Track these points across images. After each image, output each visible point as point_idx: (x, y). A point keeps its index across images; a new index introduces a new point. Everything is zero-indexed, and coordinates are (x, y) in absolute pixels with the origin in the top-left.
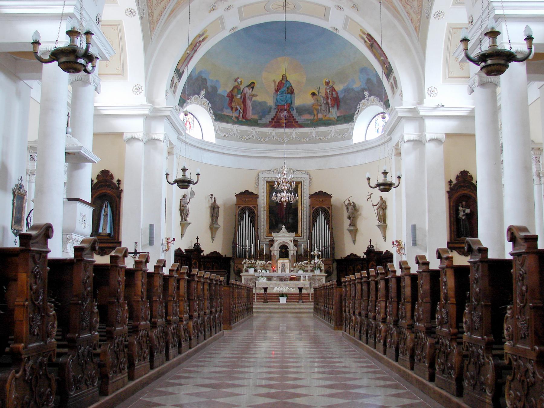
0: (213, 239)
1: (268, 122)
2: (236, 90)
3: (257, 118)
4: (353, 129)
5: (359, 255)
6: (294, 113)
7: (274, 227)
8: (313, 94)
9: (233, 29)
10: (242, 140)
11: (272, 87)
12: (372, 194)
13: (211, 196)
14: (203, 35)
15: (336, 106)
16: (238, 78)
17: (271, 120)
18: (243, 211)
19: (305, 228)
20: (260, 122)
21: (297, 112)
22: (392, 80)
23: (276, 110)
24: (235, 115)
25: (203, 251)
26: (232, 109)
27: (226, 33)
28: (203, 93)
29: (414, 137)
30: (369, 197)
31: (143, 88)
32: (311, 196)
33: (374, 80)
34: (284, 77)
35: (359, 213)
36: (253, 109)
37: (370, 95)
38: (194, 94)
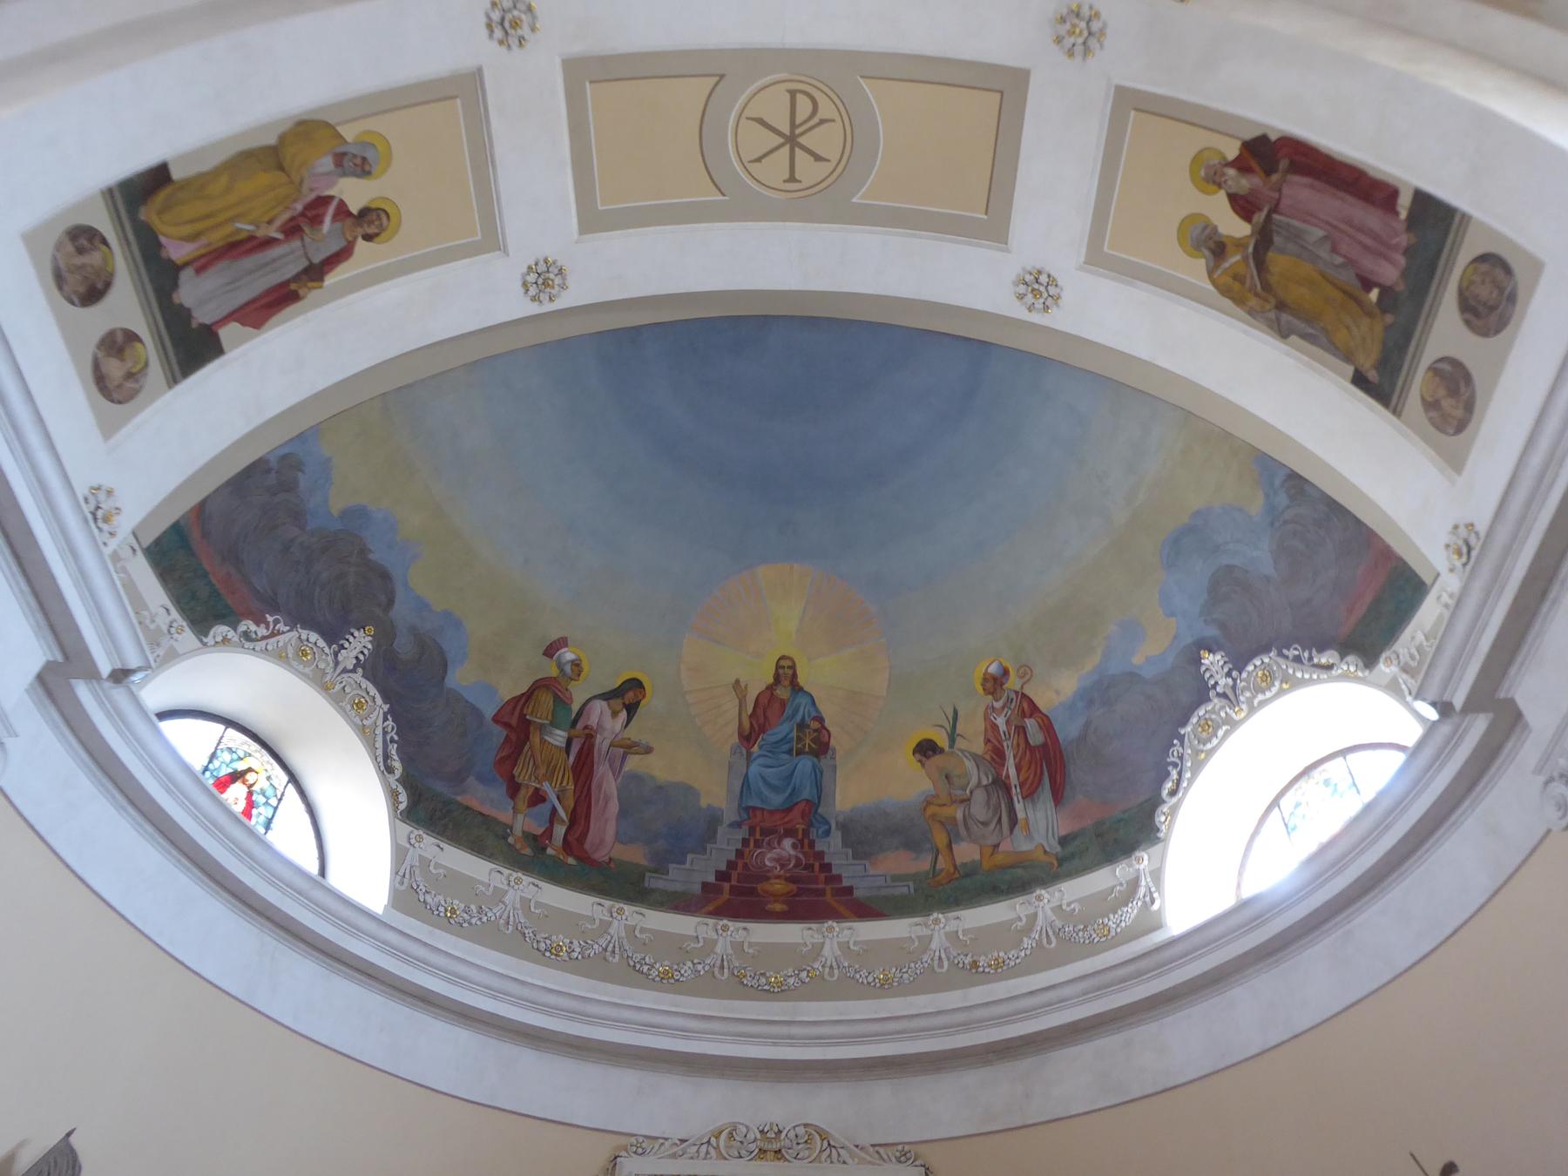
1: (697, 888)
2: (546, 700)
3: (644, 862)
4: (1157, 875)
6: (833, 847)
8: (926, 749)
11: (727, 722)
16: (562, 643)
17: (711, 879)
20: (653, 882)
21: (845, 844)
23: (742, 833)
24: (524, 822)
26: (514, 789)
28: (360, 643)
34: (786, 673)
36: (623, 813)
37: (1238, 662)
38: (301, 618)
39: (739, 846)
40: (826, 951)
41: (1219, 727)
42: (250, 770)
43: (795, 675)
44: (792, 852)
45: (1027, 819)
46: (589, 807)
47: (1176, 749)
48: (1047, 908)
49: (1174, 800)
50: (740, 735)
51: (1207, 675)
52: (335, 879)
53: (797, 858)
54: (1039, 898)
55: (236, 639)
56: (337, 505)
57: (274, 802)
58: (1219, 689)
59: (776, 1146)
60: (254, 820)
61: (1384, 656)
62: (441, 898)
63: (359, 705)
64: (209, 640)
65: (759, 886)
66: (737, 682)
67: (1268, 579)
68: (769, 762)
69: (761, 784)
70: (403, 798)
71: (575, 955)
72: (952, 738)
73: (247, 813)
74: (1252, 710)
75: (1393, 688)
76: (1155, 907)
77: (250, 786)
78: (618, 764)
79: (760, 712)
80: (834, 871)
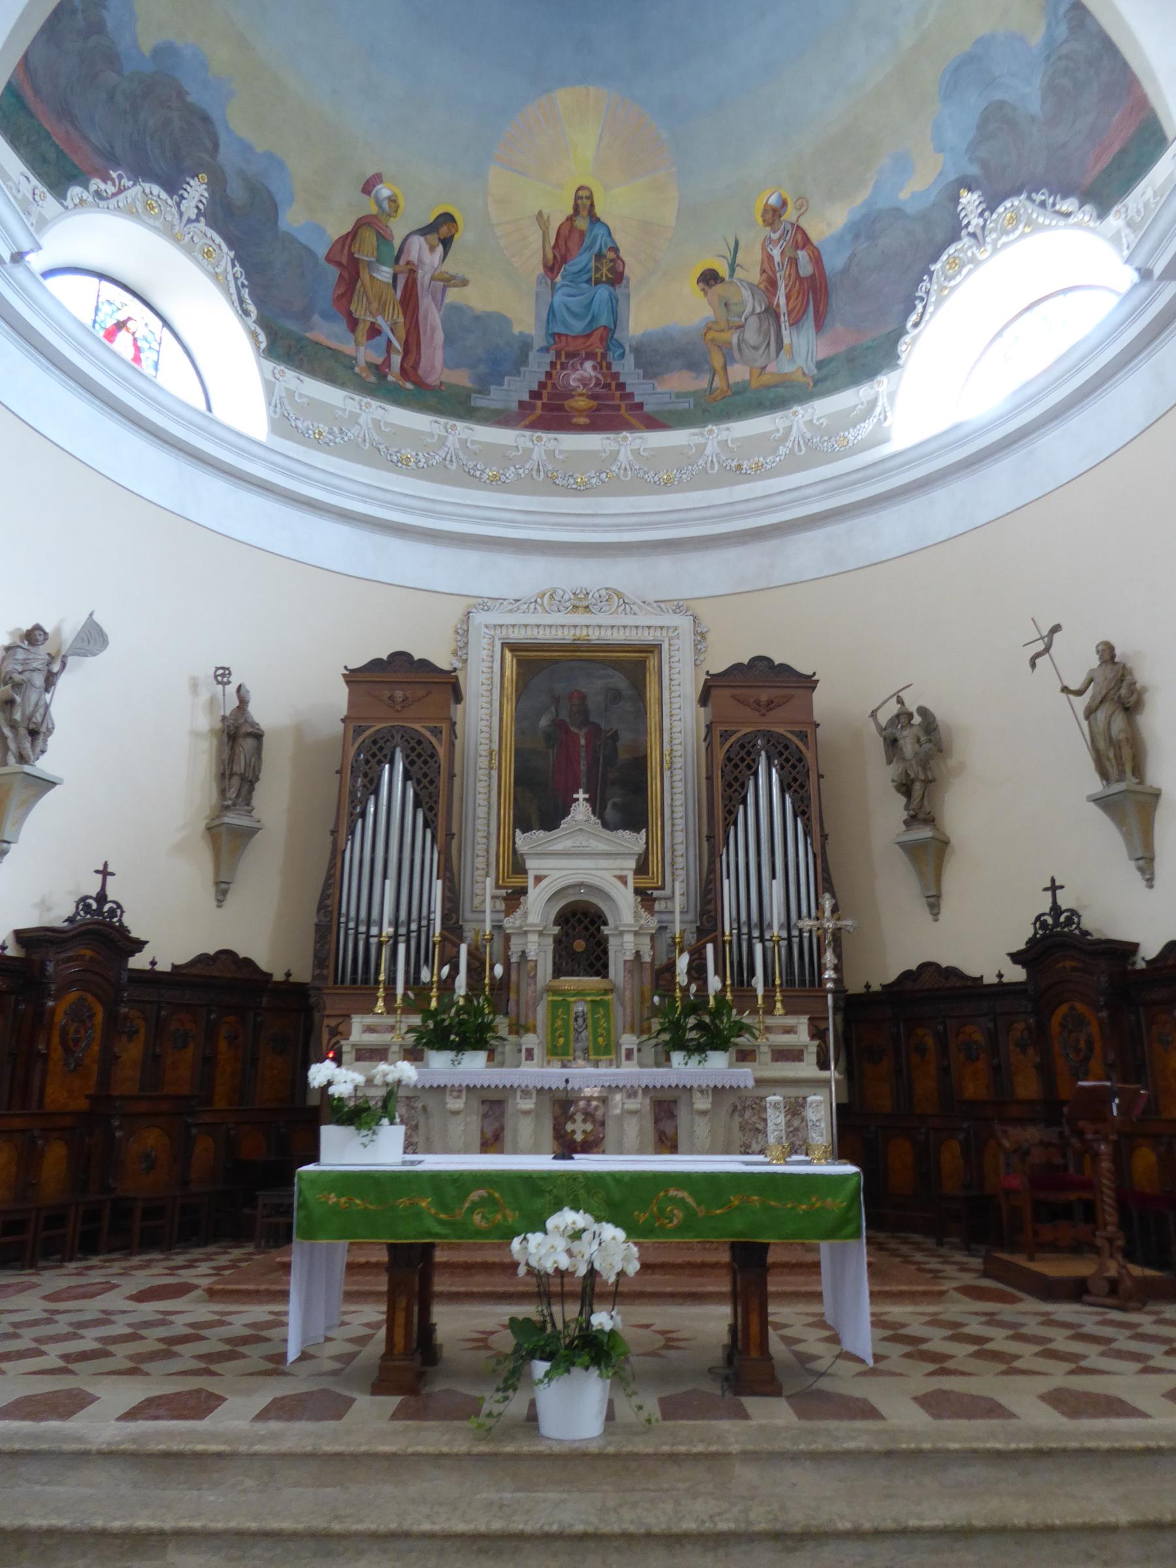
0: (222, 890)
1: (514, 406)
2: (369, 237)
3: (469, 384)
4: (892, 396)
5: (971, 969)
6: (626, 368)
7: (538, 802)
8: (709, 278)
11: (532, 253)
12: (1056, 629)
13: (223, 675)
16: (376, 179)
17: (526, 397)
18: (375, 753)
19: (681, 848)
20: (478, 401)
21: (638, 365)
23: (550, 357)
25: (139, 945)
26: (353, 324)
28: (197, 191)
30: (1040, 646)
32: (711, 689)
34: (584, 204)
35: (952, 762)
36: (449, 340)
37: (991, 203)
38: (142, 172)
39: (548, 369)
40: (621, 457)
41: (963, 266)
42: (129, 319)
43: (592, 205)
44: (593, 374)
45: (791, 345)
46: (419, 334)
47: (924, 285)
48: (801, 421)
49: (916, 331)
50: (545, 266)
51: (963, 214)
52: (219, 413)
53: (597, 379)
54: (795, 414)
55: (90, 199)
56: (147, 44)
57: (155, 346)
58: (971, 229)
59: (585, 603)
60: (144, 363)
61: (1115, 209)
62: (308, 423)
63: (209, 254)
64: (68, 203)
65: (566, 403)
66: (540, 213)
67: (1033, 118)
68: (573, 291)
69: (564, 308)
70: (262, 338)
71: (421, 464)
72: (733, 268)
73: (137, 359)
74: (995, 250)
75: (1115, 239)
76: (886, 424)
77: (133, 334)
78: (439, 296)
79: (561, 242)
80: (628, 390)
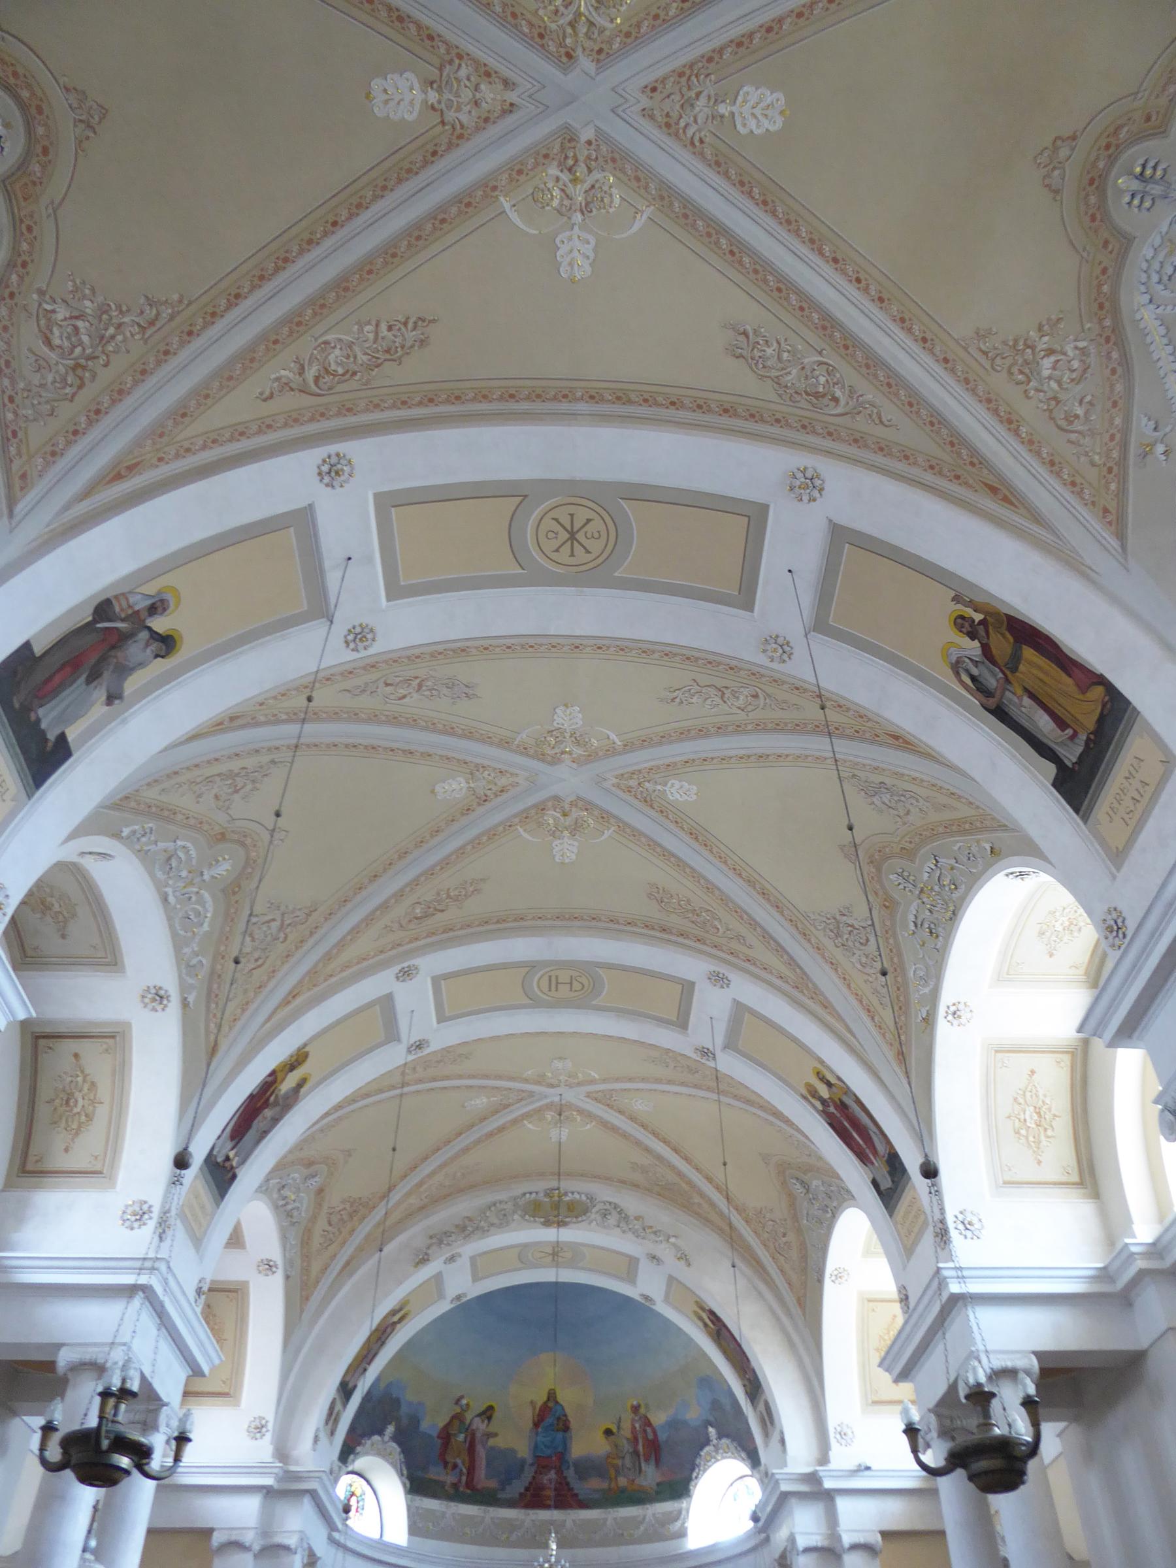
1: (517, 1496)
2: (456, 1422)
6: (570, 1474)
8: (608, 1432)
9: (458, 1297)
10: (461, 1538)
11: (528, 1416)
14: (400, 1309)
15: (653, 1462)
16: (462, 1397)
17: (522, 1490)
20: (501, 1495)
22: (761, 1407)
23: (533, 1469)
24: (449, 1479)
26: (446, 1464)
27: (444, 1307)
28: (390, 1430)
29: (816, 1540)
31: (270, 1426)
33: (725, 1401)
34: (552, 1395)
36: (489, 1463)
72: (619, 1428)
